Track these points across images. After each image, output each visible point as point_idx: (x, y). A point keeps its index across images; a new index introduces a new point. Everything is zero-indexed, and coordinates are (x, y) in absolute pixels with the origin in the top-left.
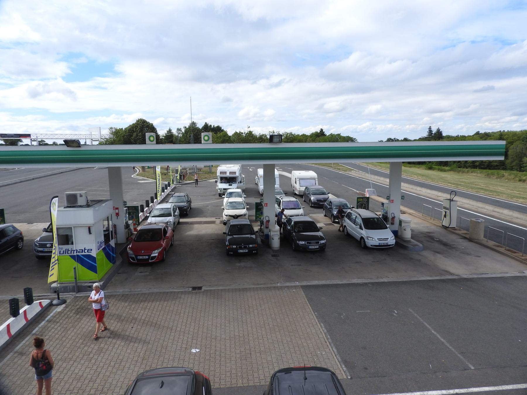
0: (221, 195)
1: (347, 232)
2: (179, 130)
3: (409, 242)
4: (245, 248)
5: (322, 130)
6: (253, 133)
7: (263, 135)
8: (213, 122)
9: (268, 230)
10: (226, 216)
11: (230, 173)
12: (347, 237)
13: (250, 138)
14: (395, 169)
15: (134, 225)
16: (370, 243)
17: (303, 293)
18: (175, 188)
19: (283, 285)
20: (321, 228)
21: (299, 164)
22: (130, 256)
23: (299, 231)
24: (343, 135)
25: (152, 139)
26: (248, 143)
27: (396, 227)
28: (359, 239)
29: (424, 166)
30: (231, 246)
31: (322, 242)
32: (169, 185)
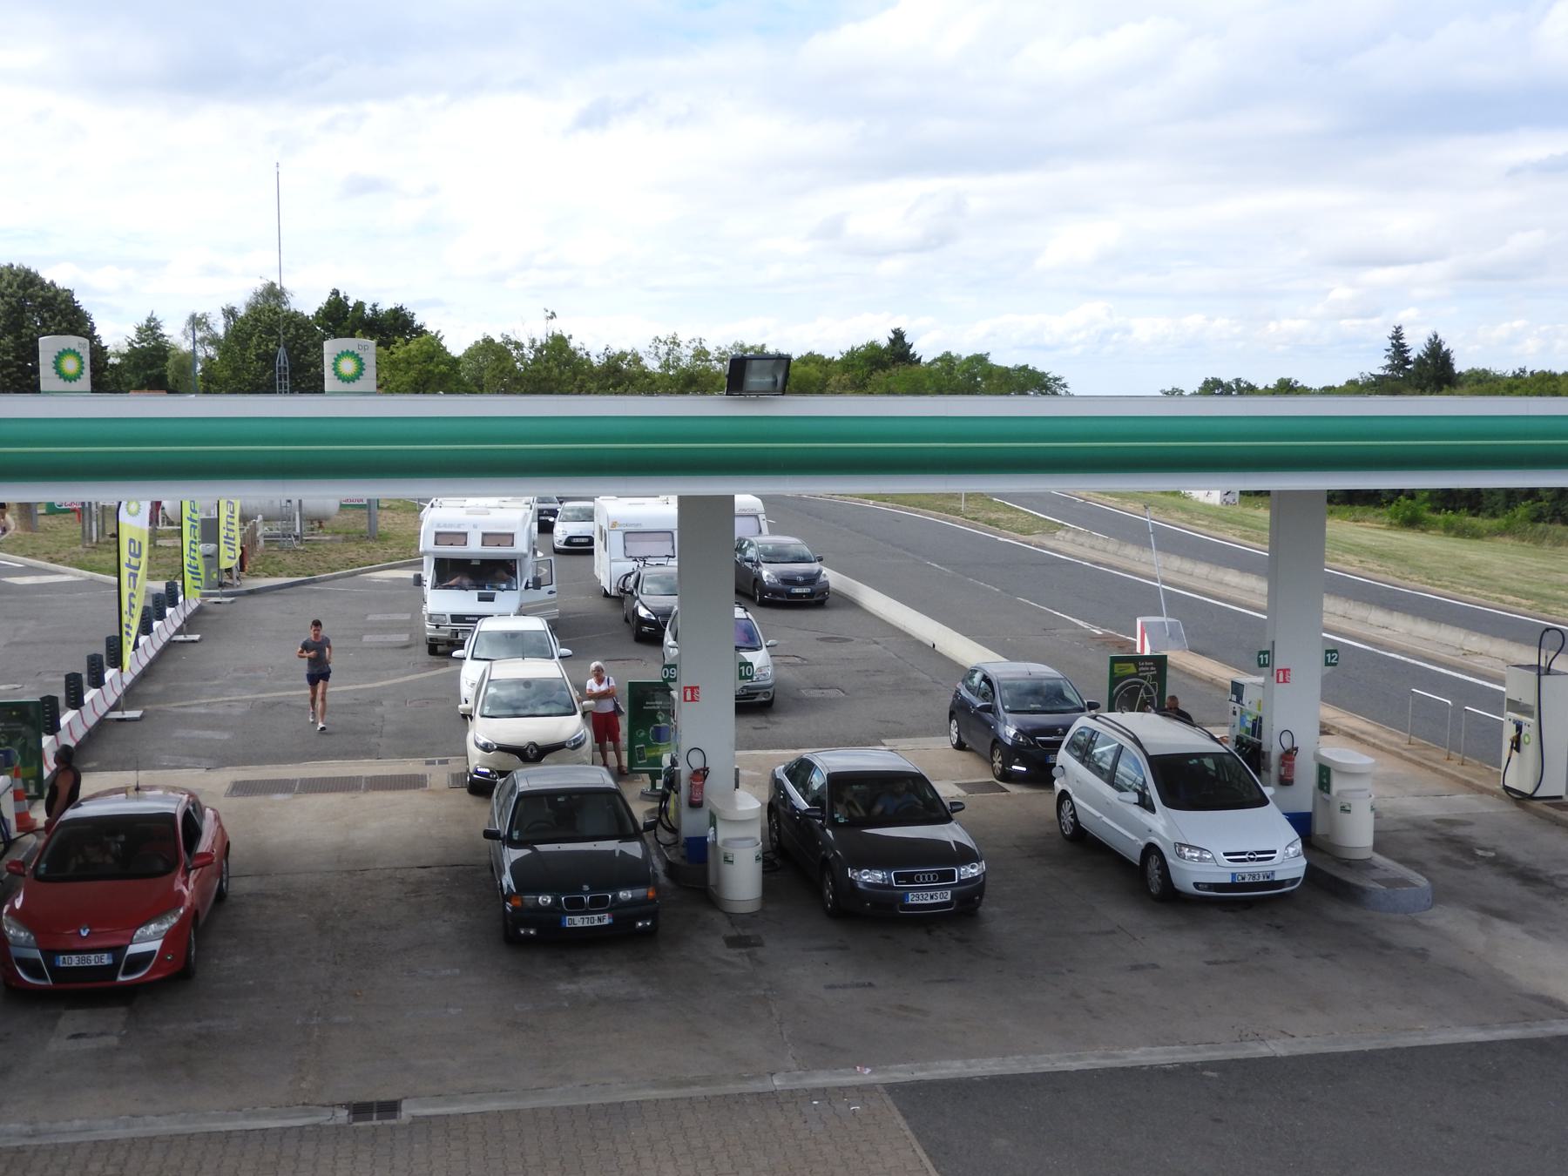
0: (444, 648)
1: (1076, 824)
2: (196, 322)
3: (1365, 865)
4: (598, 905)
5: (899, 336)
6: (573, 344)
7: (623, 355)
8: (375, 292)
9: (702, 816)
10: (486, 748)
11: (487, 538)
12: (1083, 844)
13: (558, 368)
14: (1295, 523)
15: (18, 796)
16: (1191, 873)
17: (903, 1123)
18: (199, 611)
19: (796, 1085)
20: (957, 806)
21: (800, 498)
22: (15, 952)
23: (855, 823)
24: (1003, 358)
25: (70, 365)
26: (550, 392)
27: (1303, 796)
28: (1135, 856)
29: (1385, 514)
30: (529, 898)
31: (970, 871)
32: (170, 597)
